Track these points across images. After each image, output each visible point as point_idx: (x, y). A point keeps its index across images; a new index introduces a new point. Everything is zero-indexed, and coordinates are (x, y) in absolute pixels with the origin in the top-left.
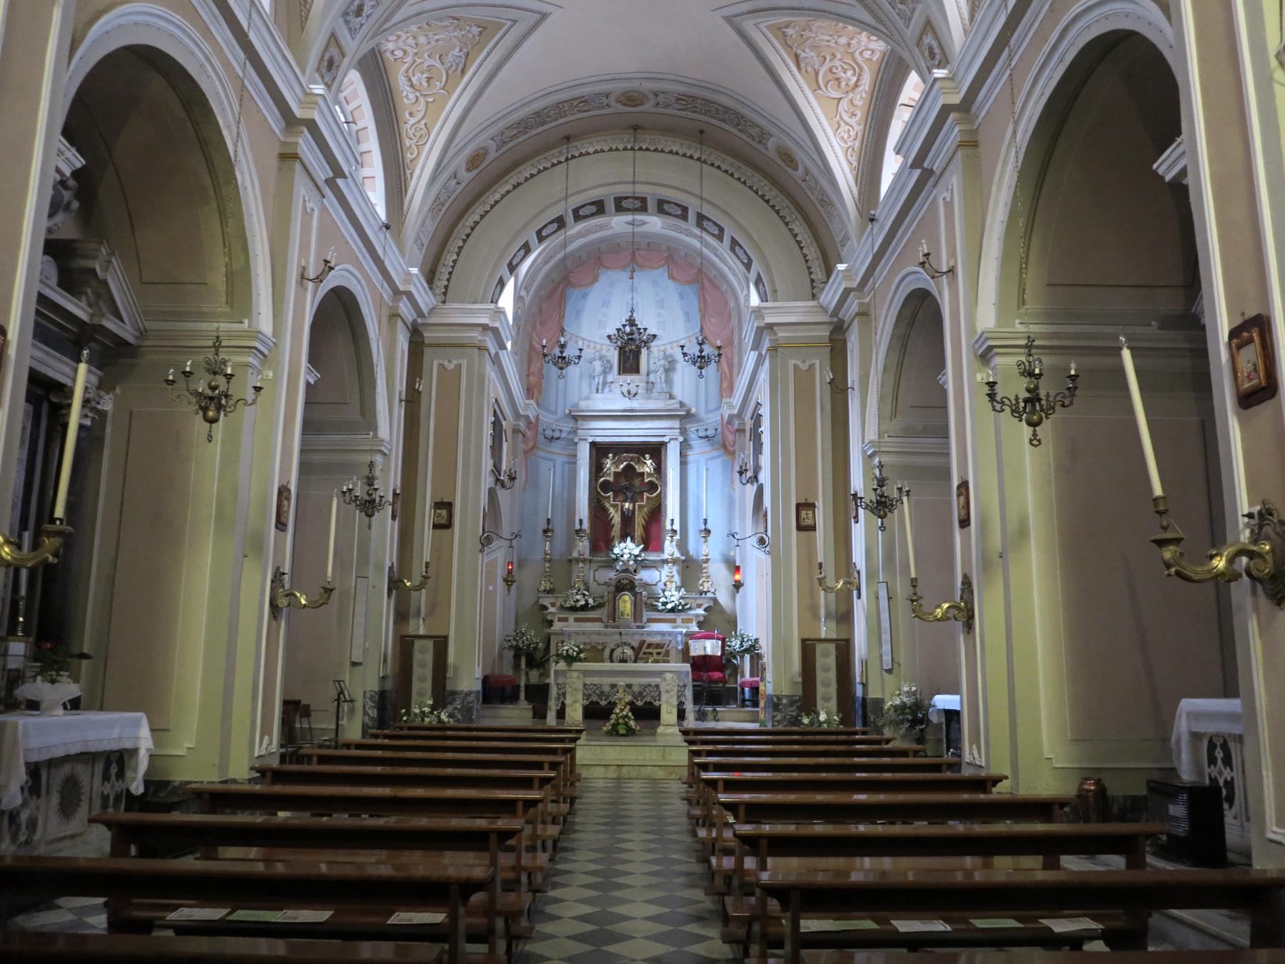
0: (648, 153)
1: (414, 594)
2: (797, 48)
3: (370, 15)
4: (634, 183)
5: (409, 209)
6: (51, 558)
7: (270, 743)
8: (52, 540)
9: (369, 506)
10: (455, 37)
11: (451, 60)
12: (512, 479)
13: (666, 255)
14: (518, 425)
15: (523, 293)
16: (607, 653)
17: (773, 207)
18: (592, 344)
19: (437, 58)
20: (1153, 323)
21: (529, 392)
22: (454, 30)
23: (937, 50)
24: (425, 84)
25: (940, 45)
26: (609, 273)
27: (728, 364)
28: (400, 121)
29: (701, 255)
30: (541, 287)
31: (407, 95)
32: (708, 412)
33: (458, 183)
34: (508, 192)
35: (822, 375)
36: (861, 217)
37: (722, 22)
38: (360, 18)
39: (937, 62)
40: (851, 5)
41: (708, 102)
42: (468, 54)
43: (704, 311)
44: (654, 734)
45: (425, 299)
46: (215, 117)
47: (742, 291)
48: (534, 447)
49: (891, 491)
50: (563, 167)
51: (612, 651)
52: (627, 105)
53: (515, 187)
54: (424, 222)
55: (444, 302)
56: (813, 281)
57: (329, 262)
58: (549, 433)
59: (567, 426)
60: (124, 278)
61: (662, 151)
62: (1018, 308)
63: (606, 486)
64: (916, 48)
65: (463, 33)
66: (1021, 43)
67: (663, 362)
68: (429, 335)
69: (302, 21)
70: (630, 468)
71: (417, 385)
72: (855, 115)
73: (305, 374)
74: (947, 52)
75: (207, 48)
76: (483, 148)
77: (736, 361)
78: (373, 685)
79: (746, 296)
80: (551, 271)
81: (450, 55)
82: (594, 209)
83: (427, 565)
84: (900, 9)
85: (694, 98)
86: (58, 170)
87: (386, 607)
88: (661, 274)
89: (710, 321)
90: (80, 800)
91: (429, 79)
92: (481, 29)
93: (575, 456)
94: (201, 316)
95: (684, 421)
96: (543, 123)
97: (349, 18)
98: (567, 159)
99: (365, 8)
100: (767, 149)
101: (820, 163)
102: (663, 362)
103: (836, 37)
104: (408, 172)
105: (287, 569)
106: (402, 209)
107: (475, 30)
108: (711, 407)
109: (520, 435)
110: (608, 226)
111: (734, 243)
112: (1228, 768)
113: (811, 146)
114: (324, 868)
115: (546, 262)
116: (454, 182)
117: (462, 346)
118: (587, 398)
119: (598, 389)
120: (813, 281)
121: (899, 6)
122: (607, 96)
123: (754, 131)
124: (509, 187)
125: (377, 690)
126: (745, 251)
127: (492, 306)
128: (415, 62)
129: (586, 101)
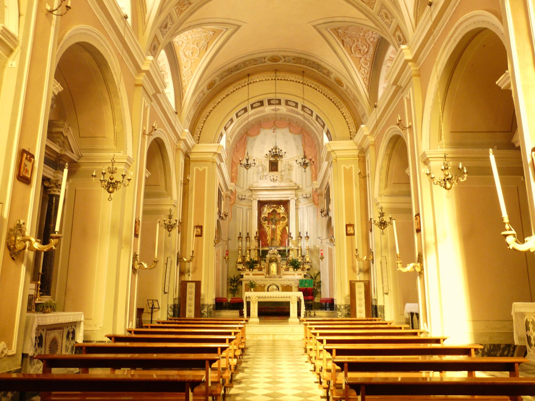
0: (281, 81)
1: (187, 264)
2: (343, 37)
3: (170, 28)
4: (276, 93)
5: (184, 106)
6: (54, 248)
7: (132, 325)
8: (55, 240)
9: (169, 227)
10: (203, 36)
11: (201, 45)
12: (226, 216)
13: (288, 122)
14: (228, 194)
15: (229, 139)
16: (266, 288)
17: (333, 102)
19: (196, 45)
20: (495, 147)
21: (232, 180)
22: (203, 33)
23: (401, 37)
24: (191, 55)
25: (403, 36)
26: (265, 130)
28: (180, 70)
29: (304, 123)
30: (236, 137)
31: (183, 60)
32: (307, 187)
33: (204, 95)
34: (224, 98)
35: (355, 170)
36: (370, 106)
37: (312, 28)
38: (166, 29)
39: (402, 42)
40: (365, 20)
41: (306, 60)
42: (208, 42)
43: (304, 145)
44: (287, 322)
45: (191, 141)
46: (111, 70)
47: (320, 137)
49: (386, 219)
50: (246, 87)
51: (268, 287)
52: (273, 62)
53: (227, 96)
54: (190, 110)
55: (198, 143)
56: (350, 132)
57: (154, 127)
58: (240, 197)
59: (248, 194)
60: (74, 135)
61: (287, 80)
62: (439, 142)
63: (266, 219)
64: (393, 37)
65: (206, 34)
66: (437, 34)
67: (287, 167)
68: (192, 156)
69: (143, 31)
71: (188, 177)
72: (367, 64)
73: (145, 173)
74: (406, 38)
75: (108, 43)
76: (214, 80)
77: (318, 166)
78: (171, 303)
79: (322, 139)
80: (241, 129)
81: (201, 43)
82: (259, 104)
83: (193, 252)
84: (386, 21)
85: (300, 58)
86: (53, 93)
87: (175, 270)
88: (286, 130)
89: (307, 150)
90: (58, 349)
91: (192, 53)
92: (213, 32)
93: (252, 206)
94: (104, 150)
95: (297, 191)
96: (238, 70)
97: (162, 29)
98: (248, 84)
99: (168, 25)
100: (330, 78)
101: (352, 83)
102: (287, 167)
103: (359, 33)
104: (184, 91)
105: (138, 253)
106: (181, 106)
107: (211, 33)
108: (308, 185)
109: (229, 198)
110: (263, 111)
111: (317, 117)
112: (529, 336)
113: (350, 77)
114: (155, 377)
115: (238, 126)
116: (202, 94)
117: (206, 161)
118: (257, 182)
119: (260, 178)
120: (350, 132)
121: (386, 20)
122: (264, 58)
123: (325, 71)
124: (225, 96)
125: (173, 304)
126: (322, 120)
127: (218, 145)
128: (187, 46)
129: (256, 60)
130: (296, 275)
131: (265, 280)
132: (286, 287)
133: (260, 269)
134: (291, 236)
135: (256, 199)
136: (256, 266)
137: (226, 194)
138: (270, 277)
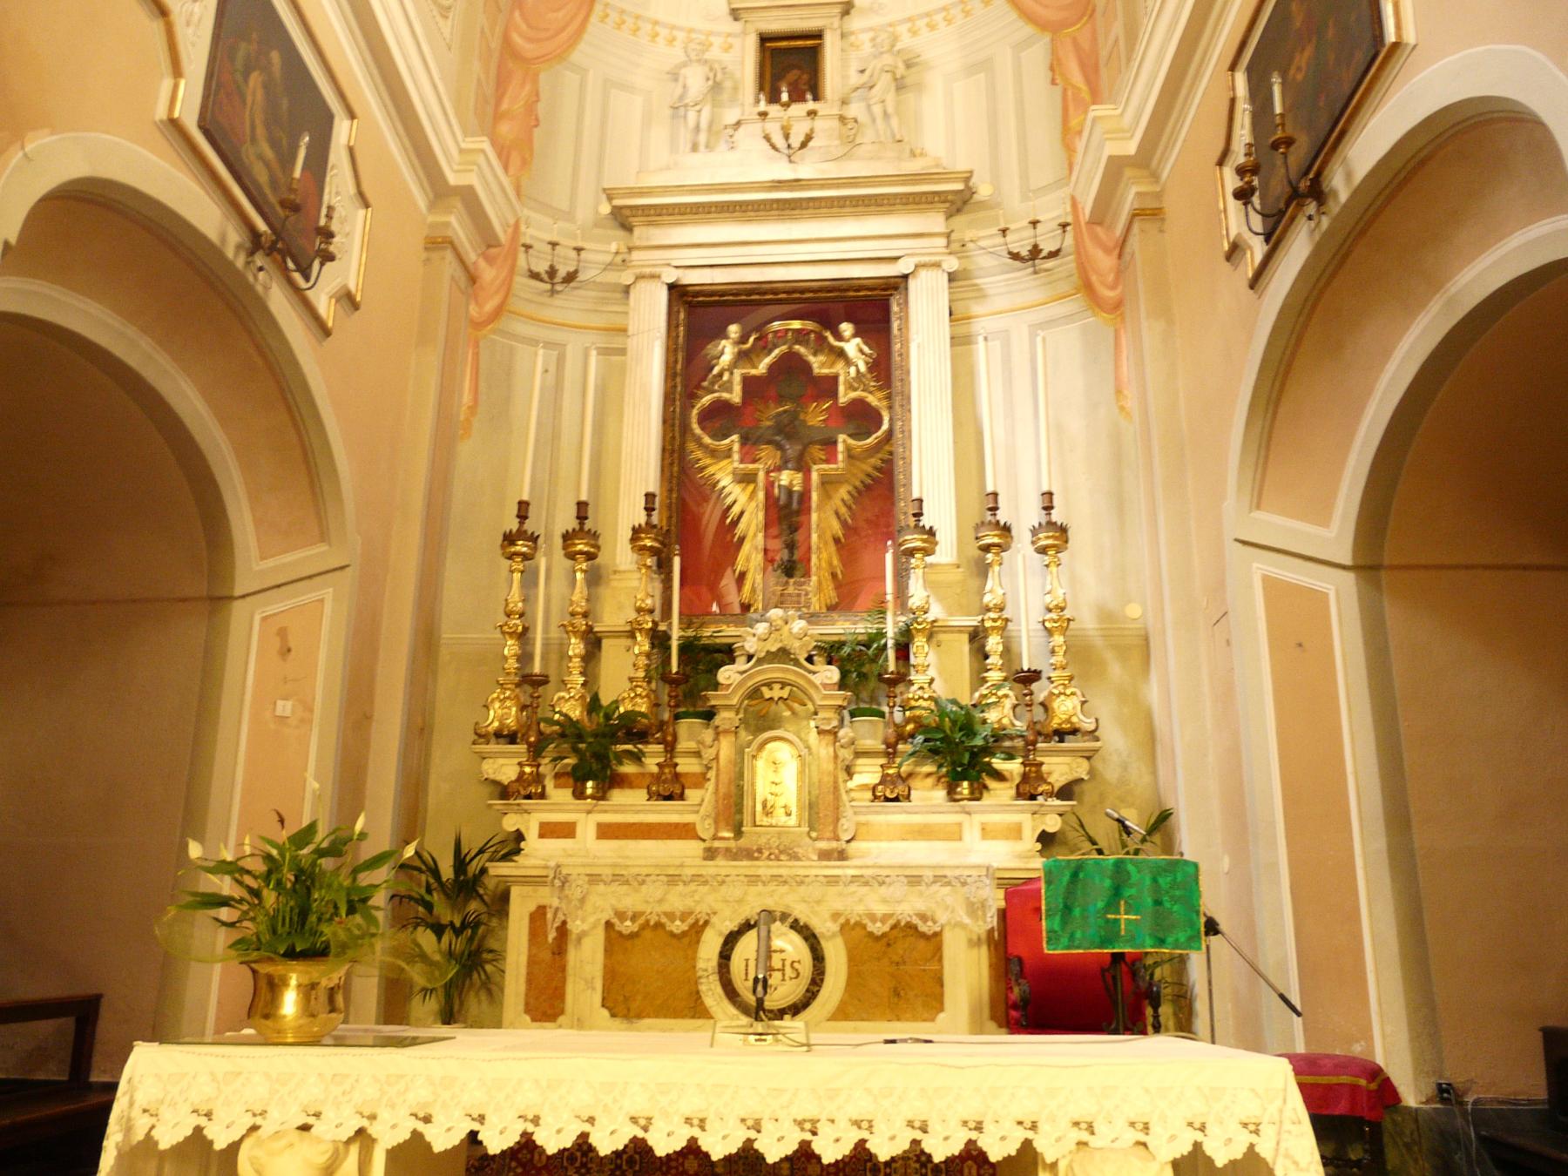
14: (447, 225)
18: (681, 36)
27: (1083, 66)
48: (498, 312)
59: (604, 247)
63: (720, 417)
67: (888, 60)
70: (791, 367)
130: (972, 833)
131: (697, 878)
132: (885, 941)
133: (670, 788)
134: (926, 521)
135: (655, 276)
136: (637, 758)
137: (433, 226)
138: (749, 854)
